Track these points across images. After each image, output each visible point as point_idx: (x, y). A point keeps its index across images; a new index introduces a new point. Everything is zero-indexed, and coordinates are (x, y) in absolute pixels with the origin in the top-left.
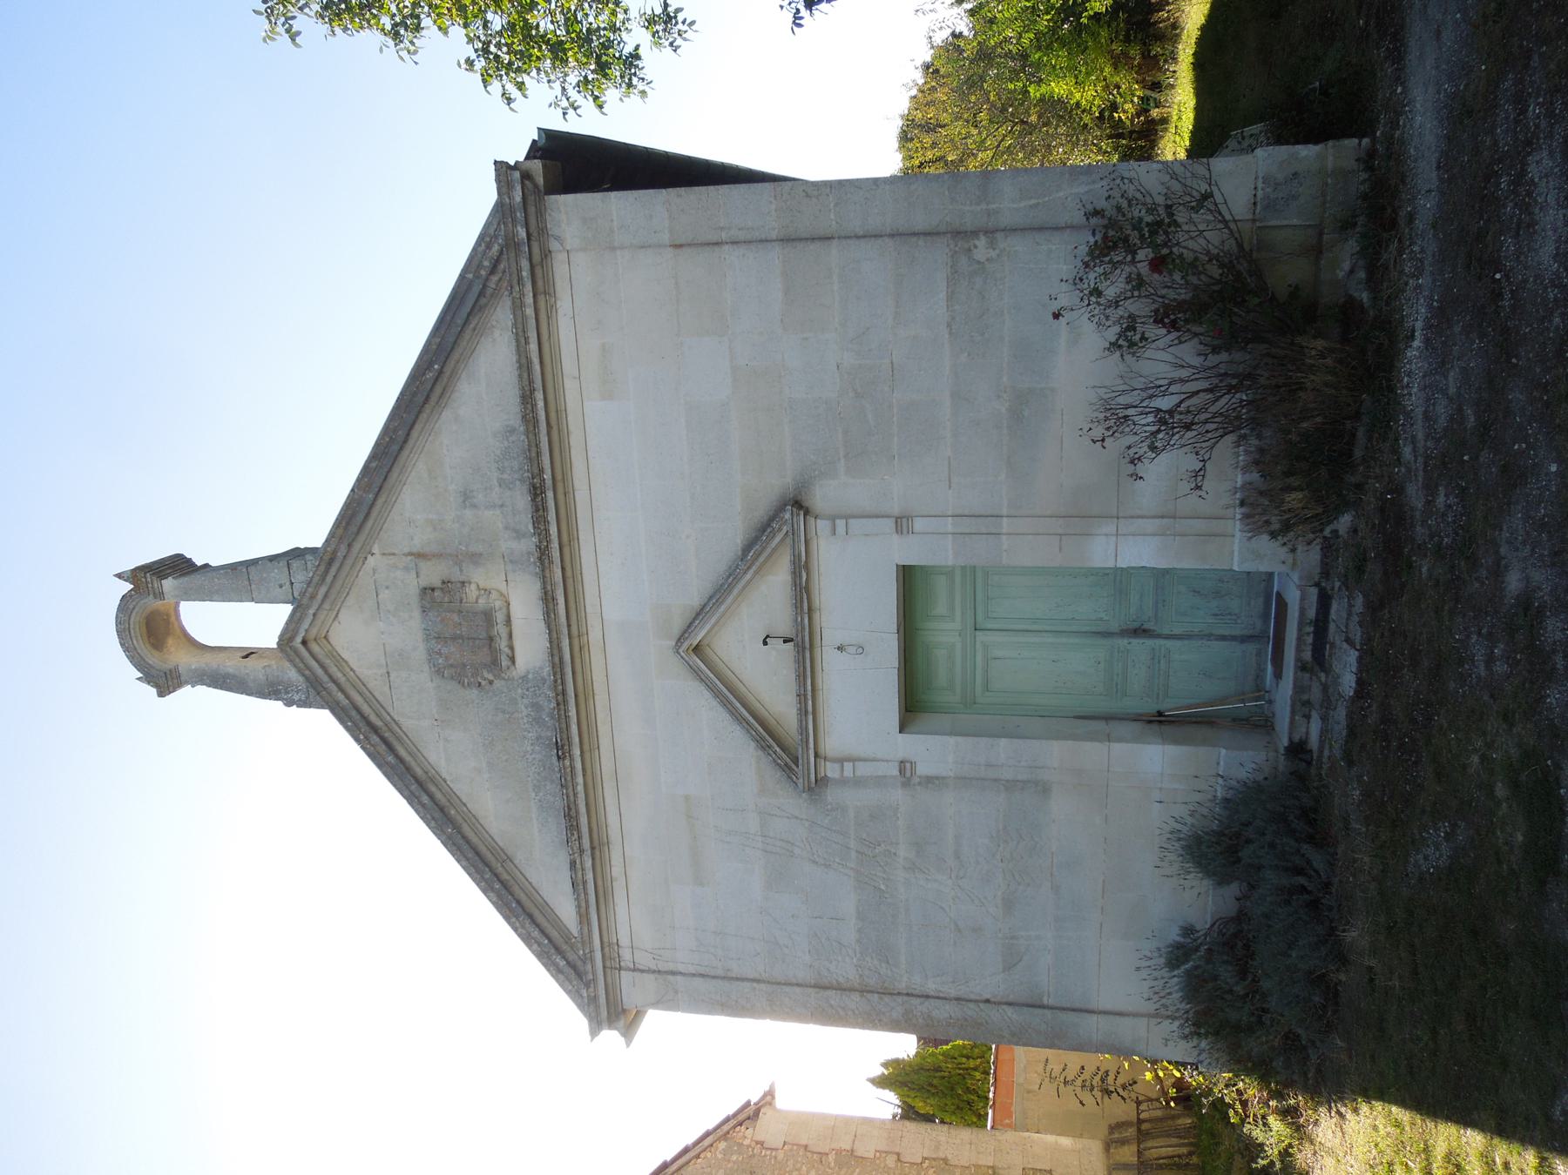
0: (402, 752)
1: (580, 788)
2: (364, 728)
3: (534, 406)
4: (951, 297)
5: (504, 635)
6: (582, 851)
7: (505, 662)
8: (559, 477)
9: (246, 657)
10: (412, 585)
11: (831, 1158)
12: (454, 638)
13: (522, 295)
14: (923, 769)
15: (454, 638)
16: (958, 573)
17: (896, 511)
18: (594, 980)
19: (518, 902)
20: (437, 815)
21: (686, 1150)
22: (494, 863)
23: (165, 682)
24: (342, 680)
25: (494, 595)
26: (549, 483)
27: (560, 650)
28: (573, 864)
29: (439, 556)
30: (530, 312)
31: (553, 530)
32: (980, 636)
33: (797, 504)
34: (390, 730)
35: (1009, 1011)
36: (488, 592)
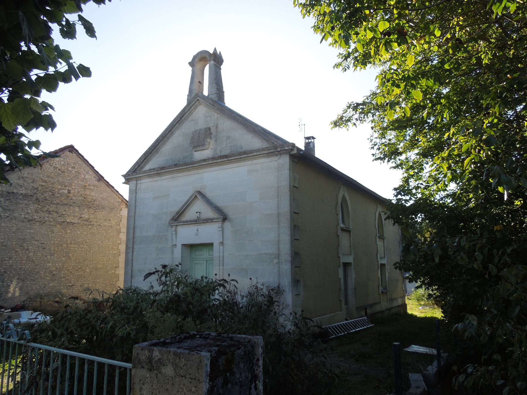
0: (177, 125)
1: (169, 170)
2: (181, 116)
3: (244, 155)
4: (266, 254)
5: (200, 149)
6: (157, 171)
7: (195, 149)
8: (230, 161)
9: (199, 82)
10: (211, 125)
11: (119, 227)
12: (199, 137)
13: (266, 150)
14: (175, 249)
15: (199, 137)
16: (212, 256)
17: (224, 242)
18: (133, 175)
19: (148, 156)
20: (164, 135)
21: (118, 192)
22: (156, 149)
23: (192, 64)
24: (191, 109)
25: (208, 146)
26: (228, 159)
27: (196, 163)
28: (154, 169)
29: (217, 132)
30: (263, 152)
31: (219, 161)
32: (205, 262)
33: (225, 219)
34: (181, 122)
35: (130, 271)
36: (209, 144)
